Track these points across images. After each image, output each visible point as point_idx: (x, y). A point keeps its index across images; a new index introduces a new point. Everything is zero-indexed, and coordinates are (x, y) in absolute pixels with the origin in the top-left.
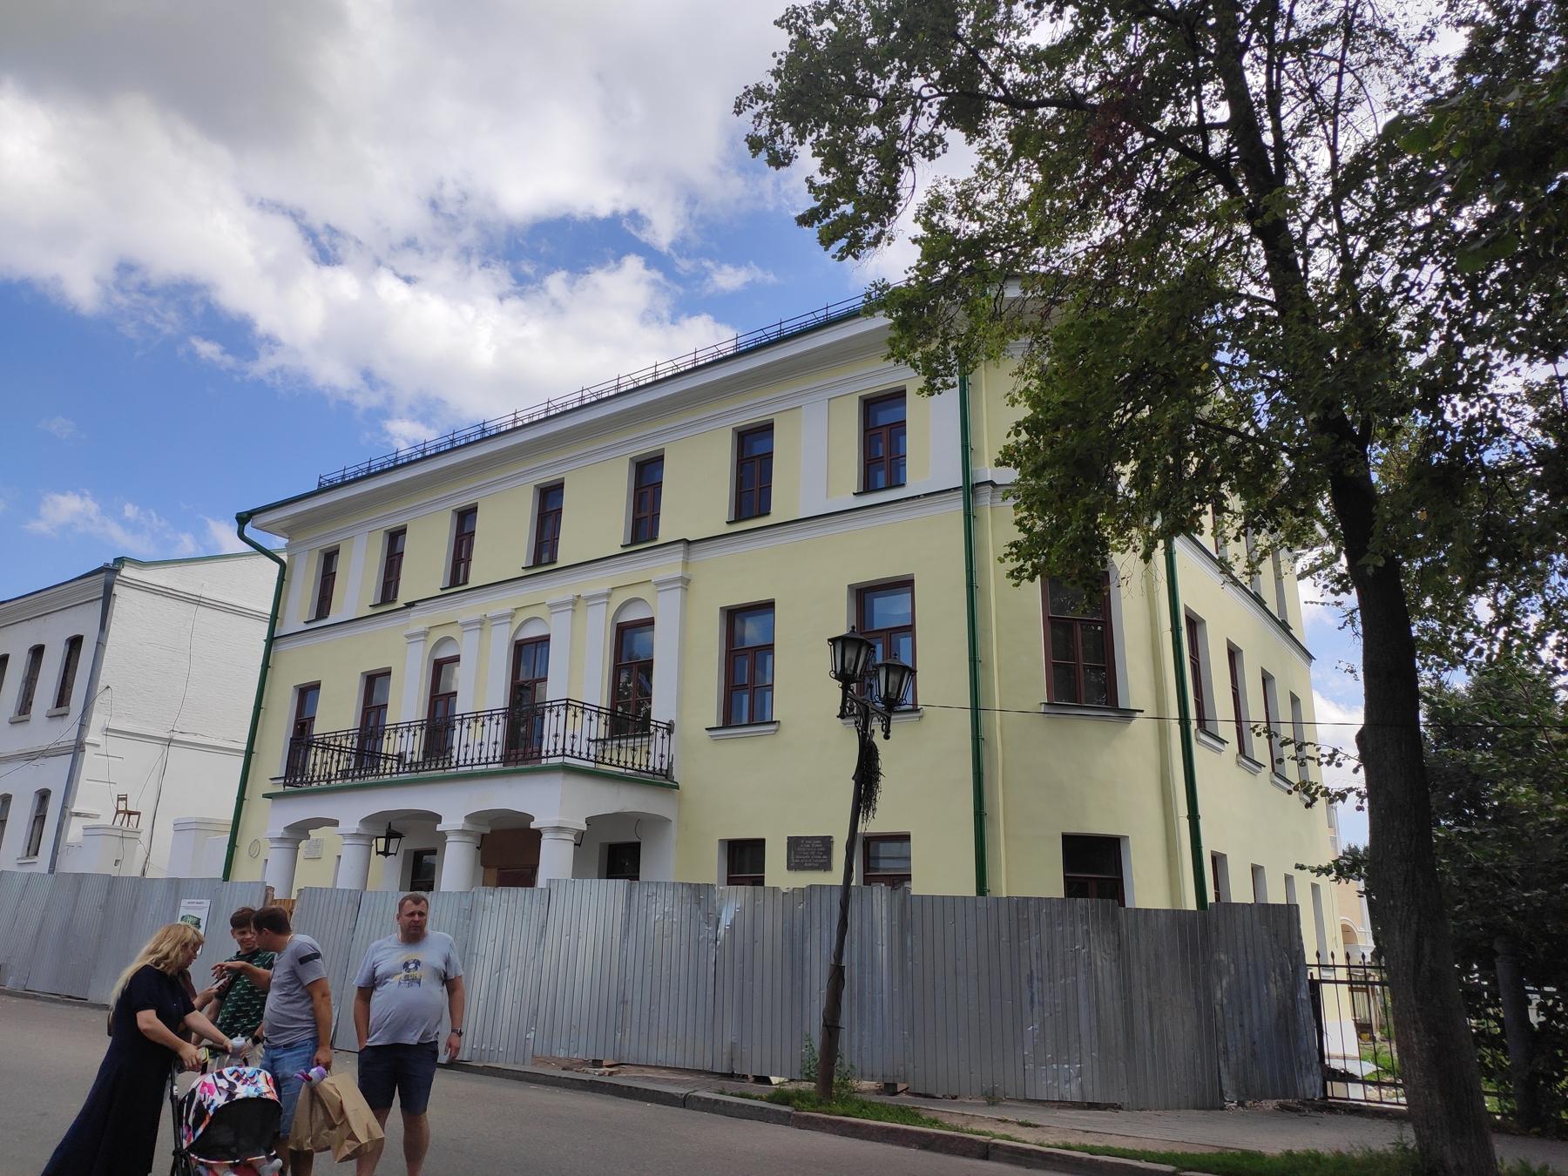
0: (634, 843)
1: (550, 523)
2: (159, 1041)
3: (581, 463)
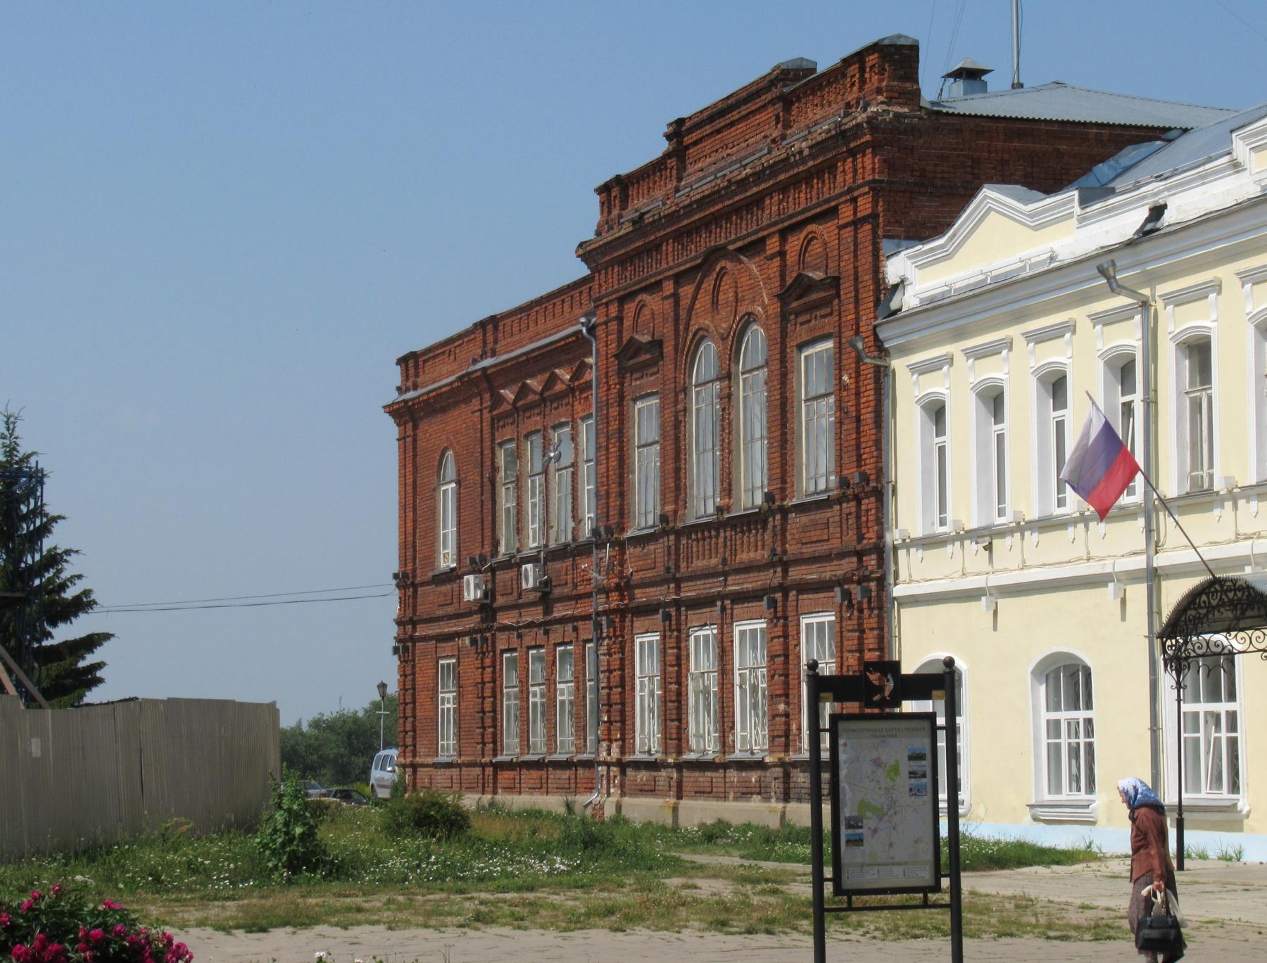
0: (1239, 788)
1: (1152, 406)
2: (956, 697)
3: (1152, 420)
